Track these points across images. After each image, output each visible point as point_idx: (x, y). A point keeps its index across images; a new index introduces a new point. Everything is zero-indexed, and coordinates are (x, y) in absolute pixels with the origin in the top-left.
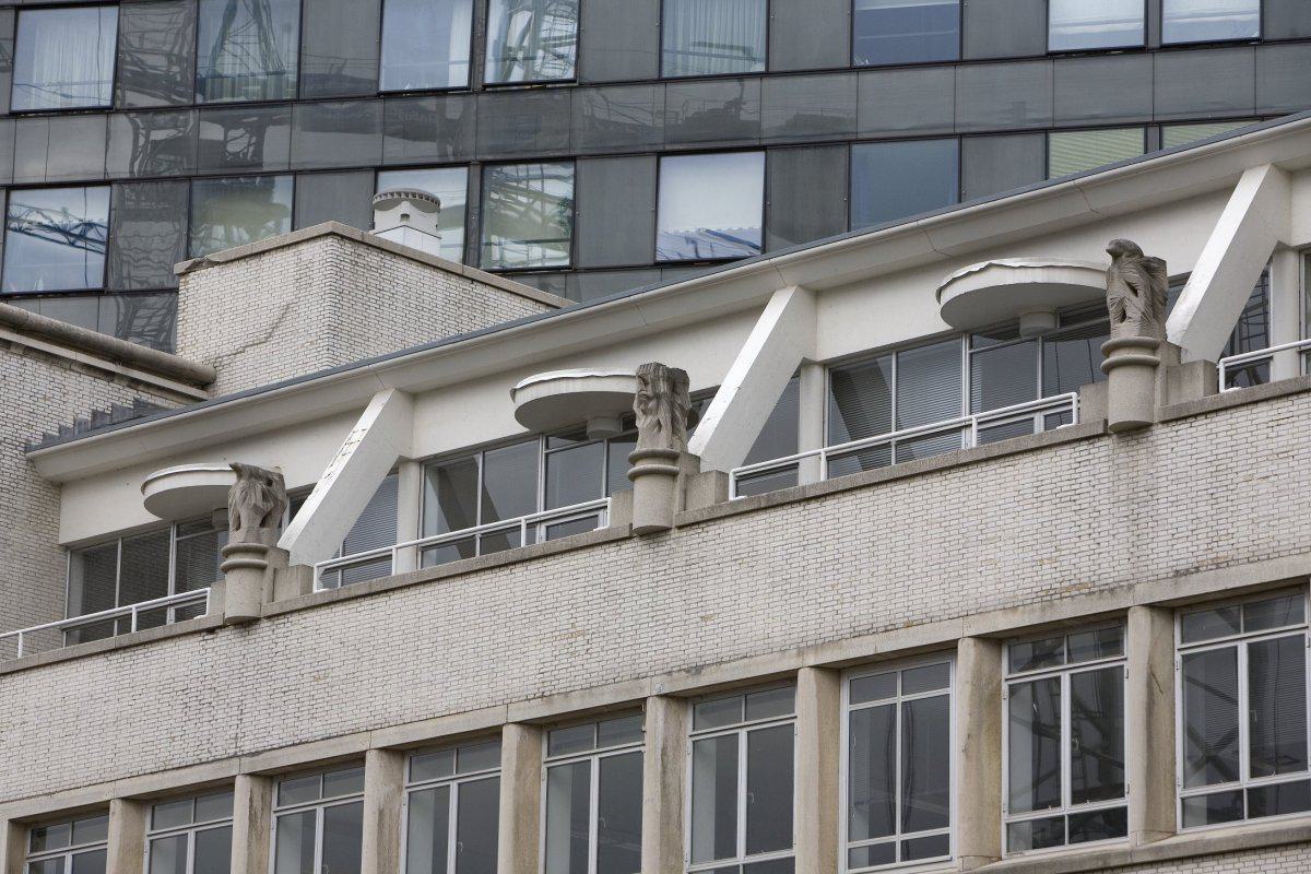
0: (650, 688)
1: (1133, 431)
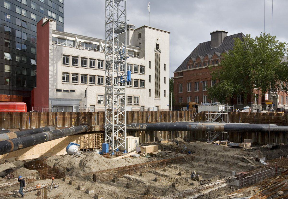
0: (140, 65)
1: (80, 49)
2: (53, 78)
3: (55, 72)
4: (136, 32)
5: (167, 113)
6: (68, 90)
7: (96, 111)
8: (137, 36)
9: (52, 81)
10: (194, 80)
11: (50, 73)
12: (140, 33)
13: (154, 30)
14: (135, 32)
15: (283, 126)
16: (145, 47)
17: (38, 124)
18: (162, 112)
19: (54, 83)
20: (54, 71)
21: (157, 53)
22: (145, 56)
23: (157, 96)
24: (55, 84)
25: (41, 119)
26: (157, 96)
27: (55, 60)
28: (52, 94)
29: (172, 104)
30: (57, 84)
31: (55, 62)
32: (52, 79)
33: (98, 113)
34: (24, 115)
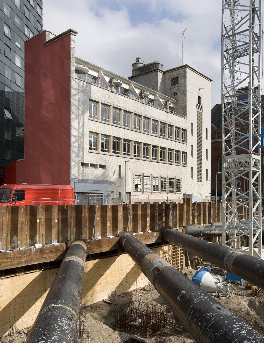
1: (112, 92)
2: (78, 142)
3: (81, 131)
4: (167, 75)
5: (207, 205)
6: (186, 152)
7: (133, 203)
8: (169, 82)
9: (76, 147)
10: (217, 157)
11: (74, 132)
12: (177, 76)
13: (196, 74)
14: (165, 75)
15: (191, 220)
16: (187, 100)
17: (101, 228)
18: (167, 206)
19: (79, 152)
20: (79, 128)
21: (199, 111)
22: (187, 114)
23: (200, 179)
24: (81, 154)
25: (107, 217)
26: (200, 179)
27: (81, 109)
28: (75, 171)
29: (216, 191)
30: (83, 153)
31: (80, 113)
32: (76, 144)
33: (135, 207)
34: (84, 209)
